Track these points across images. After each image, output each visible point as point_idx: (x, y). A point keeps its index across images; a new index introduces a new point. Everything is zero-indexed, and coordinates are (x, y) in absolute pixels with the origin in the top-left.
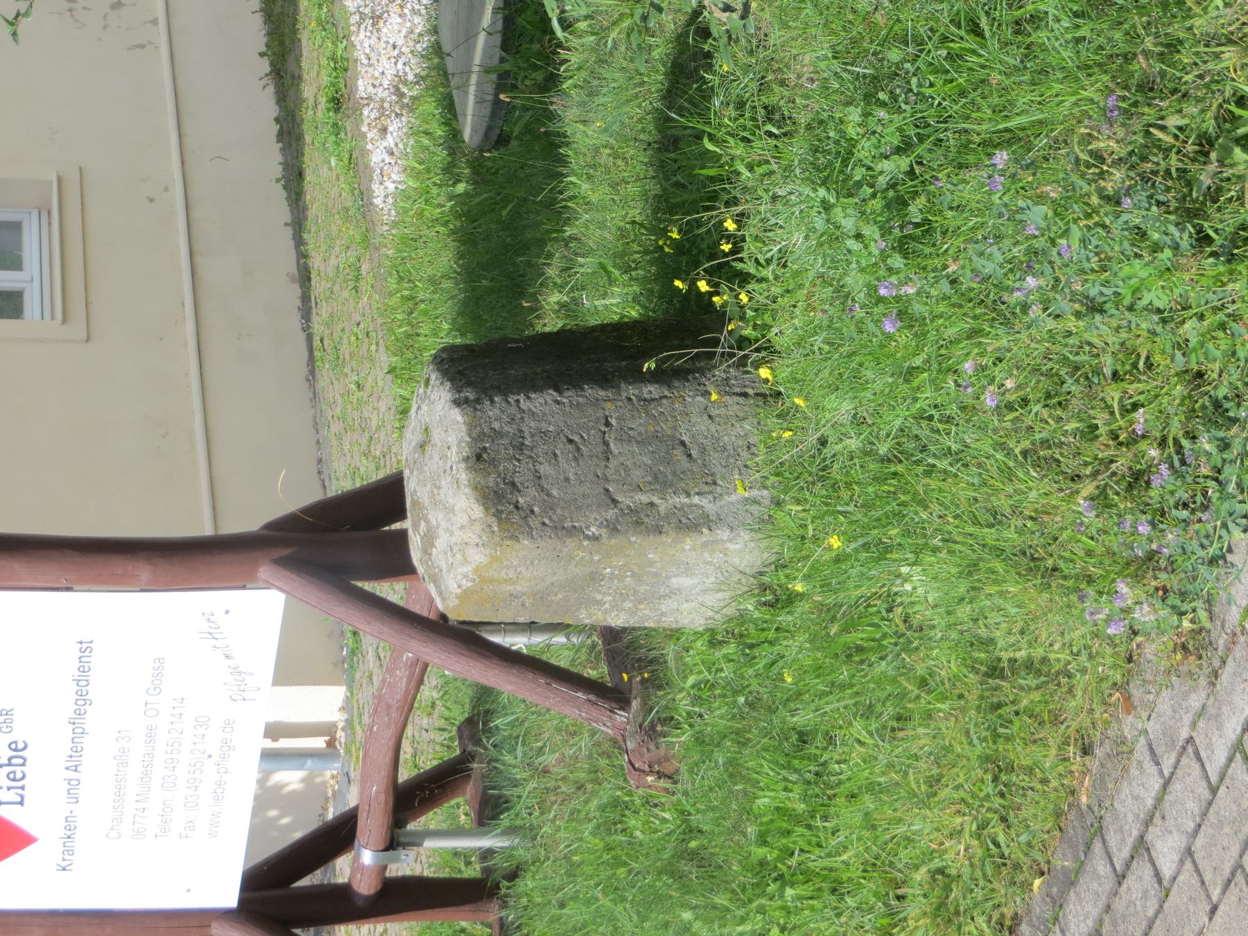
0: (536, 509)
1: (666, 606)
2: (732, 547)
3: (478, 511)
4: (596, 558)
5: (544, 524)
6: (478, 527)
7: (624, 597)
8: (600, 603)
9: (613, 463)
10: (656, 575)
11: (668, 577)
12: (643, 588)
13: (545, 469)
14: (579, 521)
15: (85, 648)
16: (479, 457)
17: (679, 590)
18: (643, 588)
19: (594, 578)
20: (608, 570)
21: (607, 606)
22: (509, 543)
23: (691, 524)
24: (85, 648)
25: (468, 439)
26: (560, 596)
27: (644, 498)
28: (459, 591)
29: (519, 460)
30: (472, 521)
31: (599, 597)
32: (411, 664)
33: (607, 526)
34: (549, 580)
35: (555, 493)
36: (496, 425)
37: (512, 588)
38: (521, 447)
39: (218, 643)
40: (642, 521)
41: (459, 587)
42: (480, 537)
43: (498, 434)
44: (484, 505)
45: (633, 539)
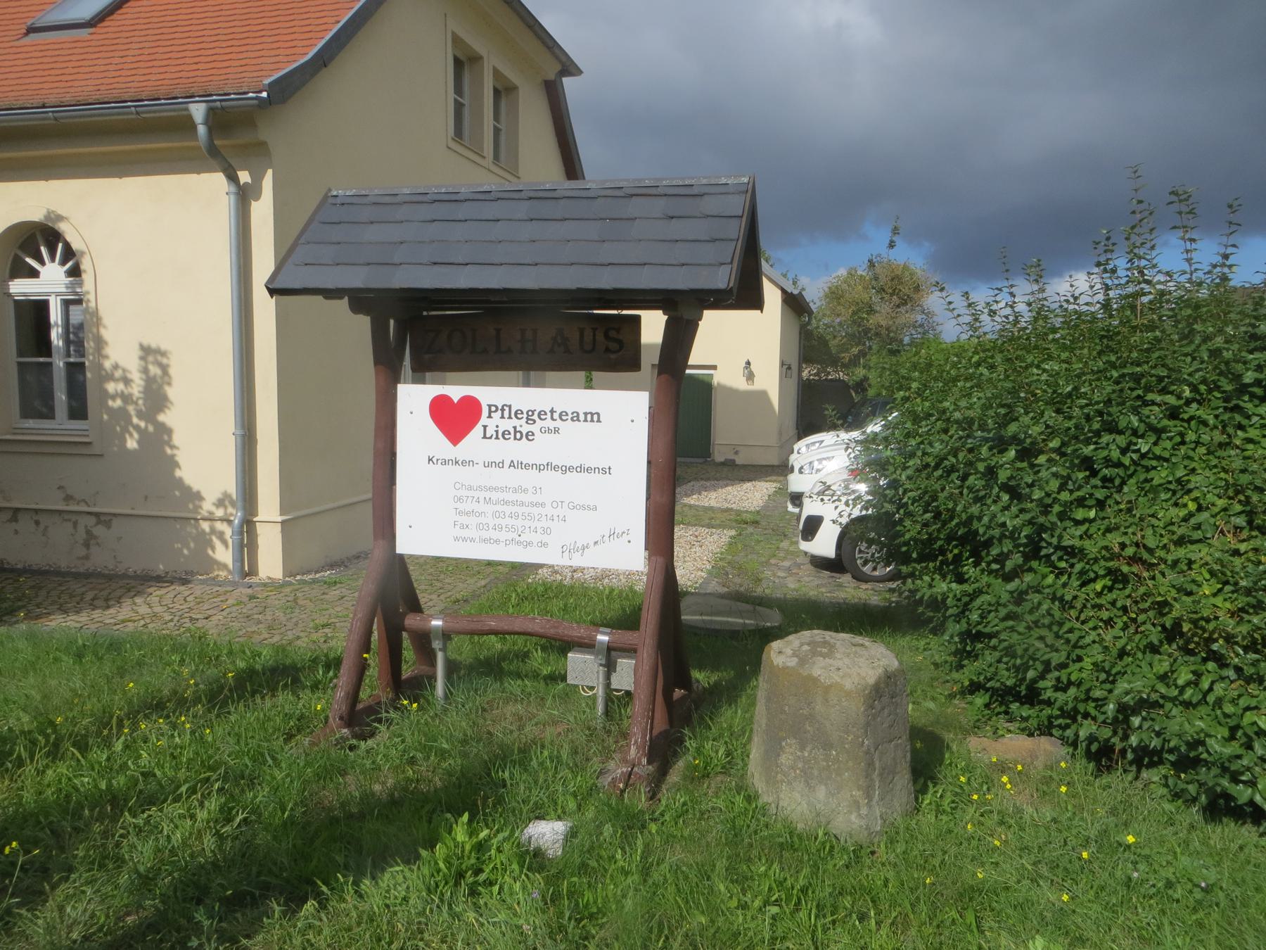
2: (853, 817)
8: (802, 749)
11: (826, 785)
12: (816, 772)
15: (607, 471)
18: (816, 772)
19: (827, 746)
24: (607, 471)
27: (877, 765)
39: (606, 538)
40: (870, 764)
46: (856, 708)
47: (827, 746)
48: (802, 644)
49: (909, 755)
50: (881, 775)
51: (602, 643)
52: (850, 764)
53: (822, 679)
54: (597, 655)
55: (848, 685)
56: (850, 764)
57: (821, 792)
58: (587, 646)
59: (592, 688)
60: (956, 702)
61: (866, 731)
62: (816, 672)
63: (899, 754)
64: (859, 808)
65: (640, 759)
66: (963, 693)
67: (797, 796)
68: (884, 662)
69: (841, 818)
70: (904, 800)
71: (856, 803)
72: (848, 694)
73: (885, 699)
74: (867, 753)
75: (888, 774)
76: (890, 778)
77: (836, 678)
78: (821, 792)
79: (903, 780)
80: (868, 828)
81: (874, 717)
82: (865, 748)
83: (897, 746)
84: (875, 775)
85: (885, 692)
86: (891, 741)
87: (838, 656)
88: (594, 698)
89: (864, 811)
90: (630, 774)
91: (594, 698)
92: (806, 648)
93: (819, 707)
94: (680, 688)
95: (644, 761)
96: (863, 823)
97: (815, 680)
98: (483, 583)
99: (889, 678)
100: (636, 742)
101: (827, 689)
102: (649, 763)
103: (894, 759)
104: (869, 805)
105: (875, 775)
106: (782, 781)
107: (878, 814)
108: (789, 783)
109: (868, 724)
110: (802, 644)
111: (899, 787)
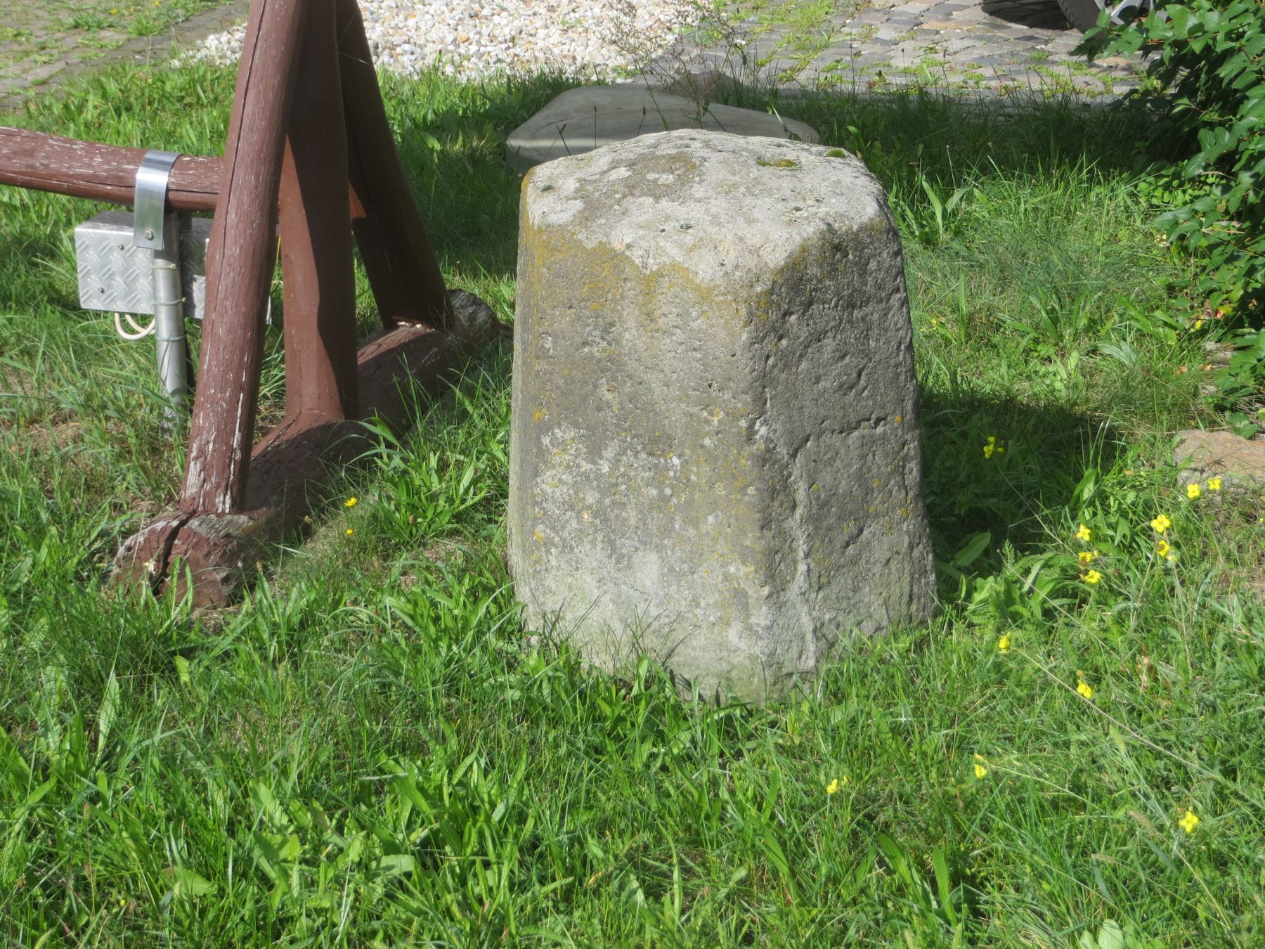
0: (784, 342)
1: (592, 554)
2: (733, 635)
3: (776, 257)
4: (707, 442)
5: (768, 357)
6: (751, 262)
7: (609, 488)
8: (595, 453)
9: (836, 440)
10: (666, 531)
11: (659, 549)
12: (632, 517)
13: (829, 344)
14: (772, 407)
16: (837, 248)
17: (629, 566)
18: (632, 517)
19: (658, 443)
20: (676, 461)
21: (586, 466)
22: (743, 312)
23: (773, 570)
25: (855, 228)
26: (609, 396)
27: (801, 495)
28: (618, 246)
29: (836, 306)
30: (755, 251)
31: (609, 453)
32: (120, 178)
33: (768, 450)
34: (651, 377)
35: (803, 365)
36: (873, 265)
37: (631, 323)
38: (851, 306)
40: (777, 492)
41: (629, 246)
42: (737, 267)
43: (863, 272)
44: (787, 266)
45: (751, 490)
46: (728, 333)
47: (658, 443)
48: (614, 165)
49: (913, 468)
50: (814, 519)
51: (148, 193)
52: (720, 490)
53: (636, 256)
54: (139, 225)
55: (705, 269)
56: (720, 490)
57: (648, 569)
58: (115, 201)
59: (144, 320)
60: (1210, 345)
61: (760, 400)
62: (622, 236)
63: (887, 458)
64: (745, 609)
65: (209, 496)
66: (1232, 325)
67: (588, 581)
68: (833, 206)
69: (700, 640)
70: (900, 588)
71: (740, 596)
72: (705, 295)
73: (825, 313)
74: (766, 458)
75: (840, 521)
76: (850, 527)
77: (672, 251)
78: (648, 569)
79: (894, 540)
80: (772, 661)
81: (787, 361)
82: (758, 447)
83: (867, 444)
84: (794, 522)
85: (817, 292)
86: (847, 429)
87: (698, 191)
88: (148, 345)
89: (761, 616)
90: (174, 533)
91: (148, 345)
92: (623, 172)
93: (631, 335)
94: (412, 319)
95: (224, 502)
96: (760, 648)
97: (615, 259)
98: (43, 73)
99: (837, 248)
100: (202, 452)
101: (650, 283)
102: (239, 506)
103: (861, 477)
104: (776, 598)
105: (794, 522)
106: (548, 544)
107: (807, 625)
108: (567, 548)
109: (764, 380)
110: (614, 165)
111: (880, 553)
